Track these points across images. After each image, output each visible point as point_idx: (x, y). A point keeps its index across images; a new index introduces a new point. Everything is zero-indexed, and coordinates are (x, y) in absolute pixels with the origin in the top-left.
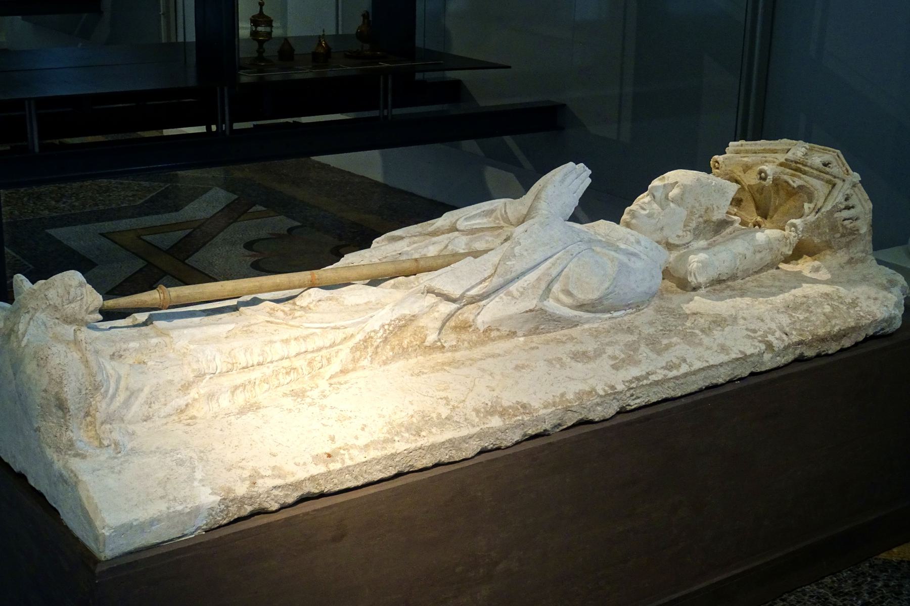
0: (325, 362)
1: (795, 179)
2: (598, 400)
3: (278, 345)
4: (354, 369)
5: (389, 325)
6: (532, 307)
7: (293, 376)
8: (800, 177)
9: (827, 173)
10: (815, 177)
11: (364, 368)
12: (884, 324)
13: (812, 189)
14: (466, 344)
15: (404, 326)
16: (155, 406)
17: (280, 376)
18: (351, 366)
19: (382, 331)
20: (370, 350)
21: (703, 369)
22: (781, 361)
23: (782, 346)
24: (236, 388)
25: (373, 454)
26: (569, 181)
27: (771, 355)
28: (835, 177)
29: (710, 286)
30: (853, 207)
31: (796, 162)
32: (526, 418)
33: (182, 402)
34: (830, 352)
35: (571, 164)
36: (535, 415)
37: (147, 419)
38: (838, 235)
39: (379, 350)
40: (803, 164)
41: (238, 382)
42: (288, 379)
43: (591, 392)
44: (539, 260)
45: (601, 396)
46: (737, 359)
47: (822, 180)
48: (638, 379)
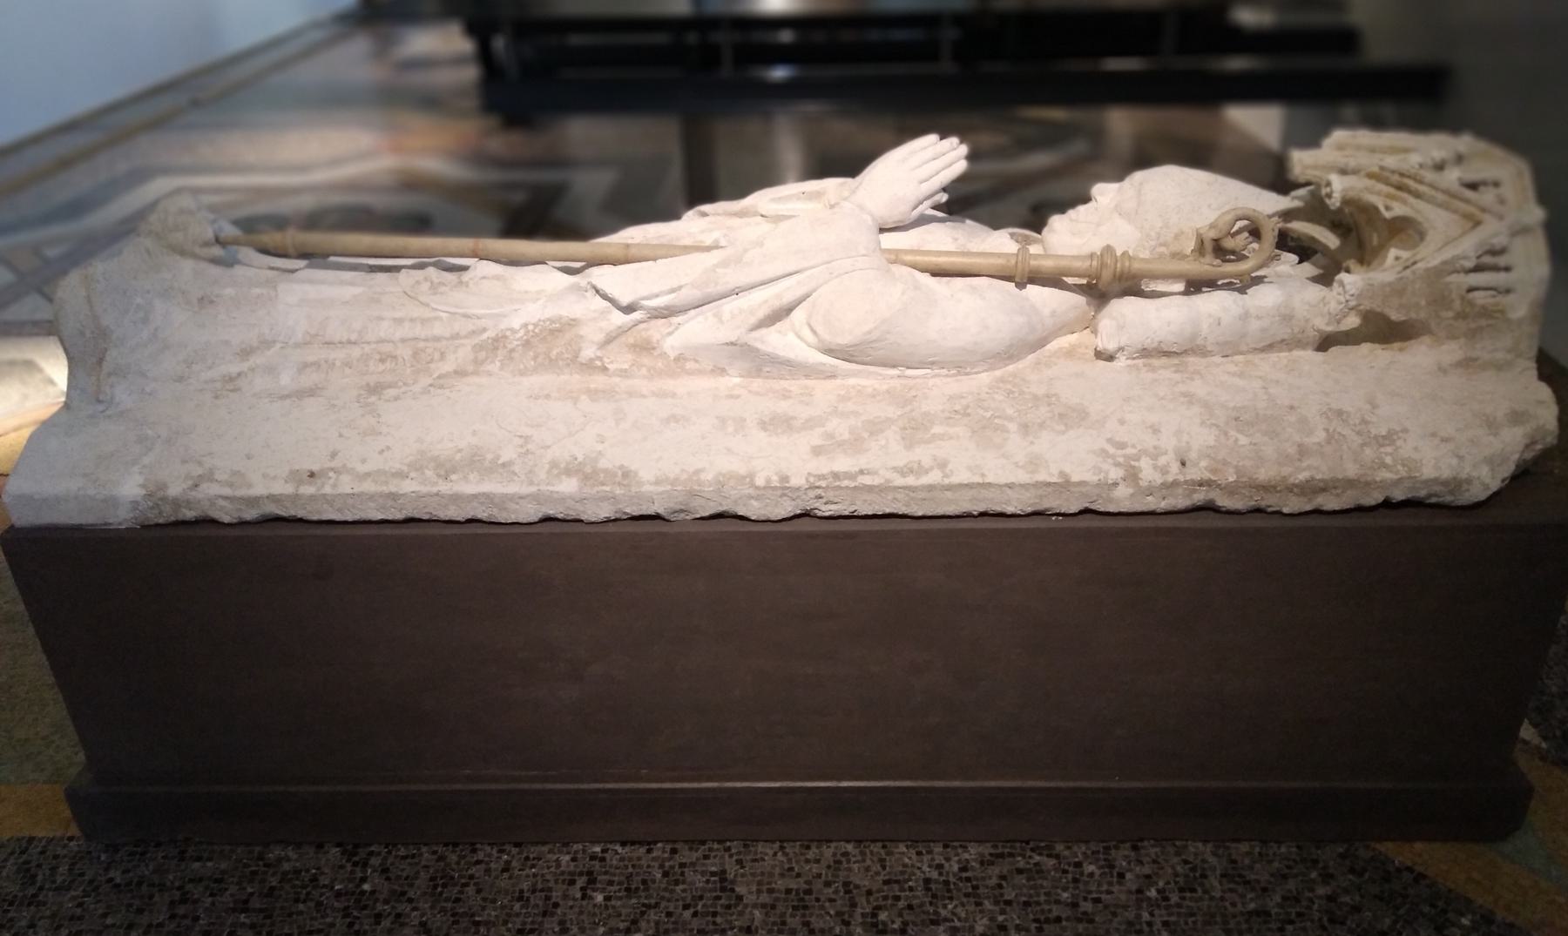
0: (437, 356)
1: (1395, 204)
2: (751, 491)
3: (385, 324)
4: (476, 373)
5: (536, 325)
6: (733, 339)
7: (388, 365)
8: (1404, 202)
9: (1467, 201)
10: (1440, 205)
11: (490, 374)
12: (1437, 488)
13: (1426, 225)
14: (644, 371)
15: (559, 331)
16: (195, 367)
17: (371, 363)
18: (471, 368)
19: (522, 332)
20: (501, 353)
21: (969, 486)
22: (1151, 503)
23: (1159, 481)
24: (306, 365)
25: (369, 487)
26: (928, 161)
27: (1131, 491)
28: (1484, 210)
29: (1143, 357)
30: (1507, 269)
31: (1402, 175)
32: (618, 491)
33: (234, 369)
34: (1286, 510)
35: (932, 138)
36: (634, 489)
37: (180, 379)
38: (1451, 314)
39: (515, 355)
40: (1415, 180)
41: (311, 359)
42: (381, 367)
43: (744, 478)
44: (770, 275)
45: (757, 488)
46: (1049, 484)
47: (1455, 211)
48: (836, 476)
